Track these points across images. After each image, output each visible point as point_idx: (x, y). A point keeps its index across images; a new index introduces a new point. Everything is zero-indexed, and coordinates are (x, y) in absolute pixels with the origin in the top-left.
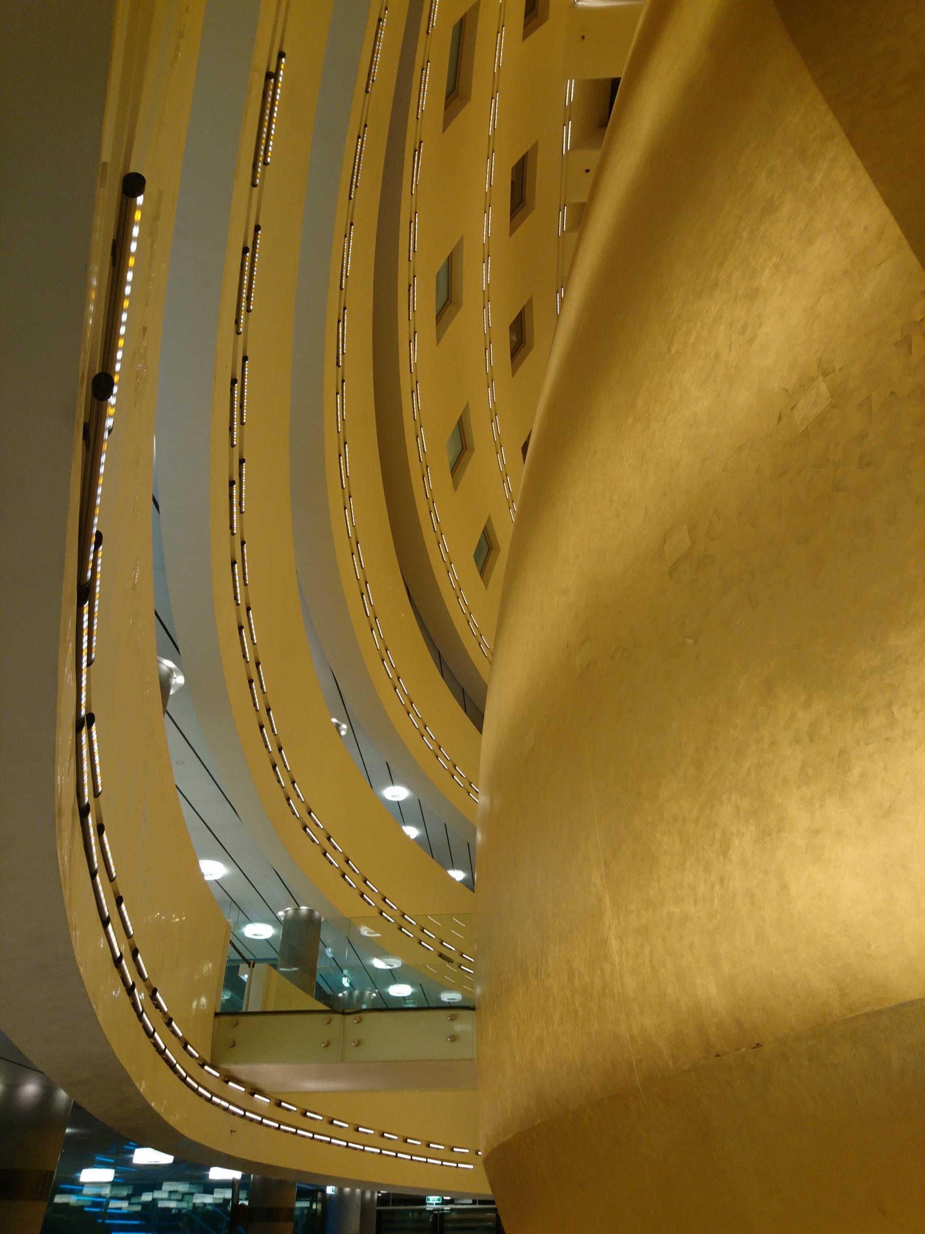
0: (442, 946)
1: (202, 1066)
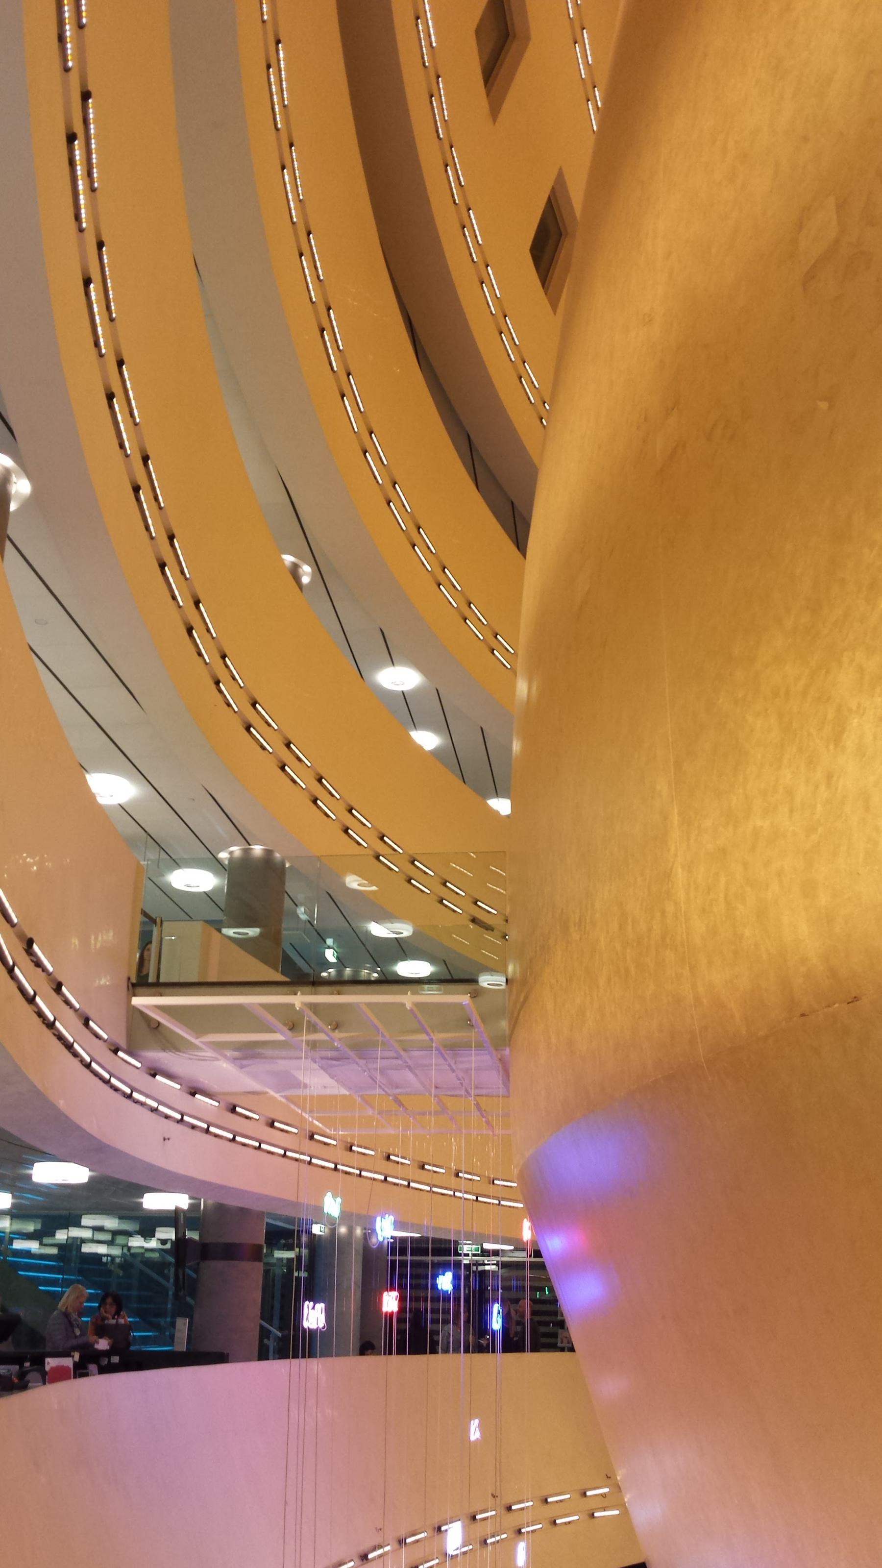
0: (382, 844)
1: (115, 1051)
